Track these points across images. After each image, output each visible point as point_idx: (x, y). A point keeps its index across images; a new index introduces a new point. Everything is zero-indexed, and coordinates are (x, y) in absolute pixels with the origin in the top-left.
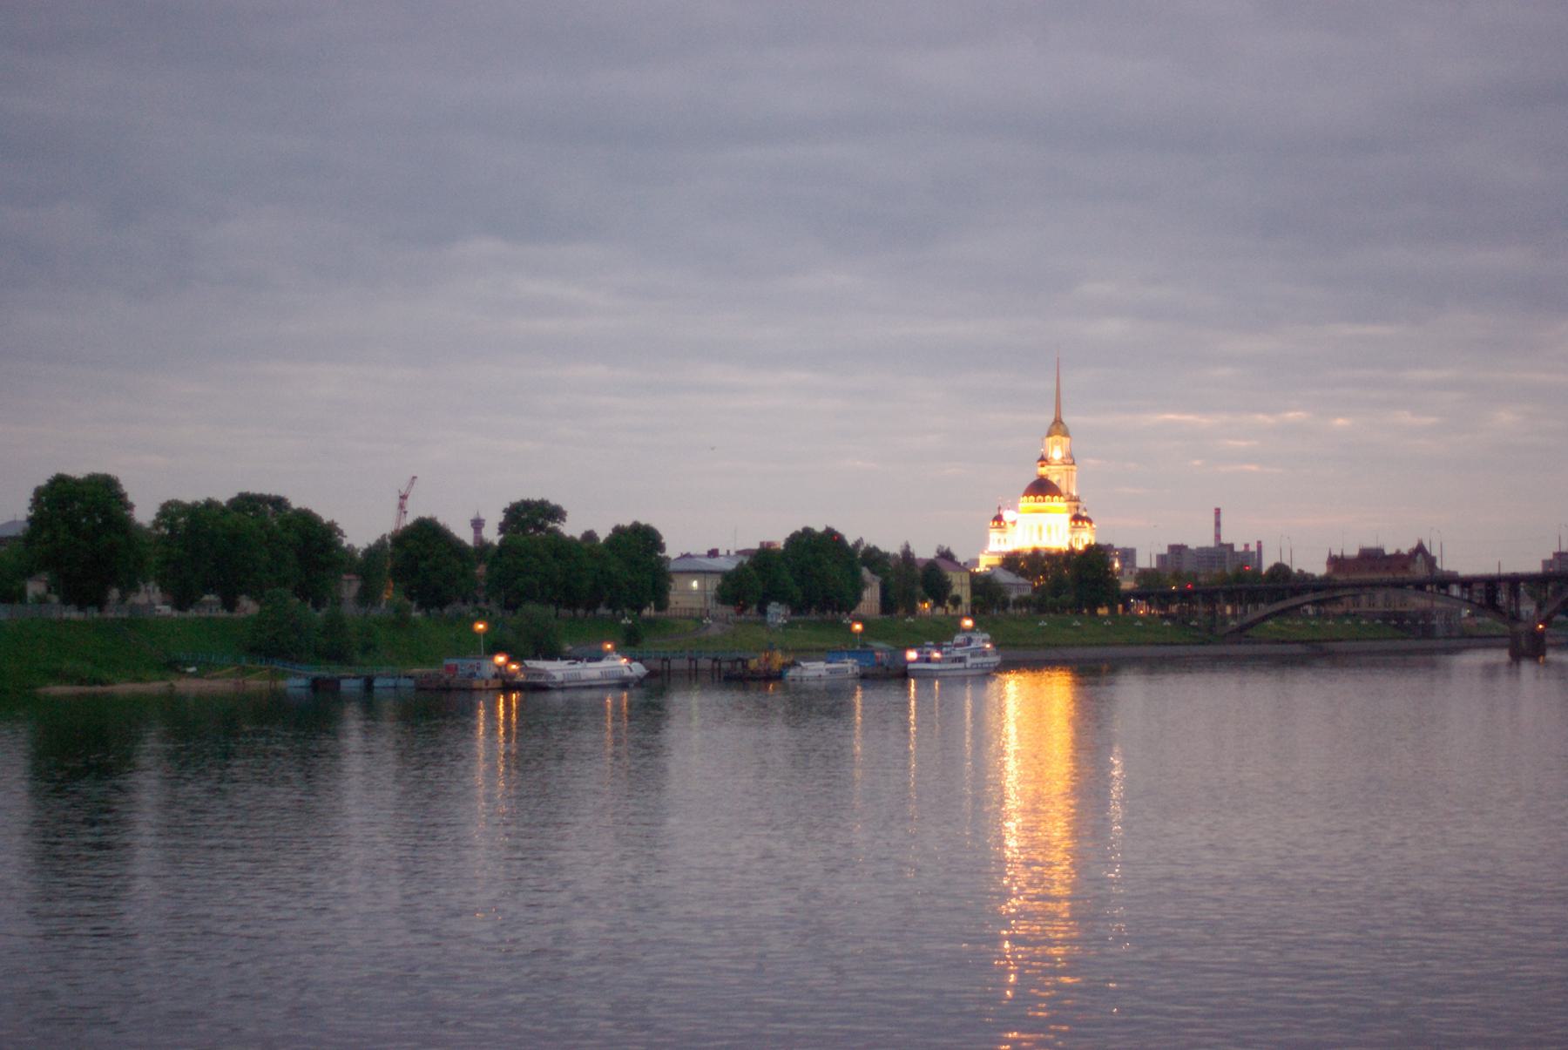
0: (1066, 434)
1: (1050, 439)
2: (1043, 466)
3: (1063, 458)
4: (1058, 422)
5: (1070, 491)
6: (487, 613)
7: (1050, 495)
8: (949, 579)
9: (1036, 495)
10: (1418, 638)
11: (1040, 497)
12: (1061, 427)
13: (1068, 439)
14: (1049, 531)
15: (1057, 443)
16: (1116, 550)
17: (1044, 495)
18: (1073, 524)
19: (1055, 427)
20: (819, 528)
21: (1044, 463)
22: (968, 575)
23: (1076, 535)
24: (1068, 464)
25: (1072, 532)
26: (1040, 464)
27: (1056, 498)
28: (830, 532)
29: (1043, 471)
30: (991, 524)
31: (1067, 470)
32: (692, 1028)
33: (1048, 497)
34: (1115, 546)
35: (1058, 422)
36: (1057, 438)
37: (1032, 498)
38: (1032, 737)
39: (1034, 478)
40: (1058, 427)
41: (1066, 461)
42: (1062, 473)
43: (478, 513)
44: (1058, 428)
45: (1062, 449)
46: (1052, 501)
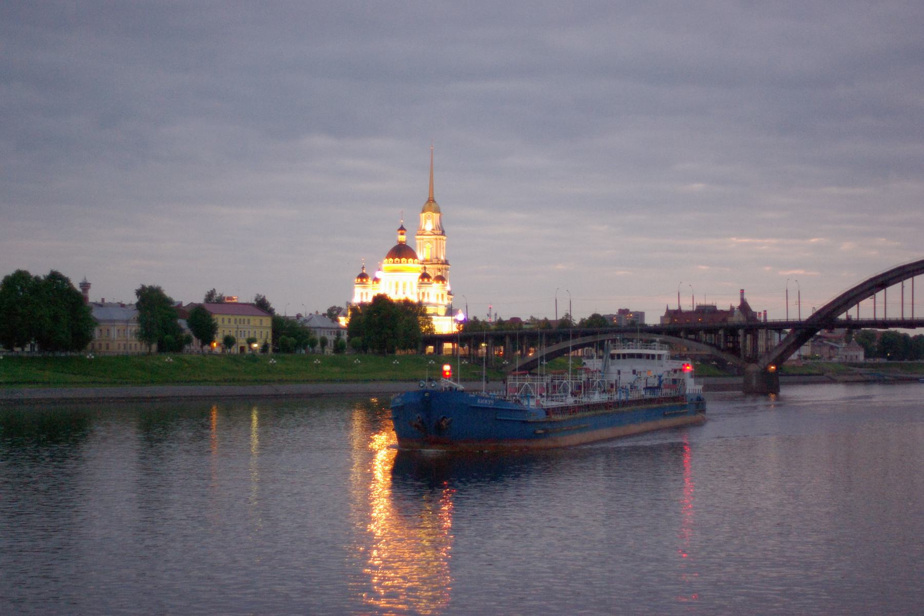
0: (437, 211)
1: (424, 214)
2: (402, 234)
3: (433, 230)
4: (431, 200)
5: (439, 257)
6: (412, 340)
7: (406, 258)
8: (215, 321)
9: (393, 258)
10: (733, 376)
11: (397, 259)
12: (433, 205)
13: (439, 215)
14: (404, 286)
15: (428, 218)
16: (631, 313)
17: (400, 257)
18: (421, 280)
19: (428, 204)
20: (376, 295)
21: (403, 231)
22: (267, 322)
23: (423, 290)
24: (437, 235)
25: (420, 287)
26: (400, 232)
27: (411, 260)
28: (55, 277)
29: (402, 238)
30: (356, 280)
31: (436, 239)
32: (682, 411)
33: (403, 259)
34: (631, 311)
35: (431, 200)
36: (429, 213)
37: (391, 260)
38: (363, 456)
39: (394, 244)
40: (431, 204)
41: (436, 232)
42: (432, 242)
43: (85, 279)
44: (430, 205)
45: (433, 224)
46: (407, 262)
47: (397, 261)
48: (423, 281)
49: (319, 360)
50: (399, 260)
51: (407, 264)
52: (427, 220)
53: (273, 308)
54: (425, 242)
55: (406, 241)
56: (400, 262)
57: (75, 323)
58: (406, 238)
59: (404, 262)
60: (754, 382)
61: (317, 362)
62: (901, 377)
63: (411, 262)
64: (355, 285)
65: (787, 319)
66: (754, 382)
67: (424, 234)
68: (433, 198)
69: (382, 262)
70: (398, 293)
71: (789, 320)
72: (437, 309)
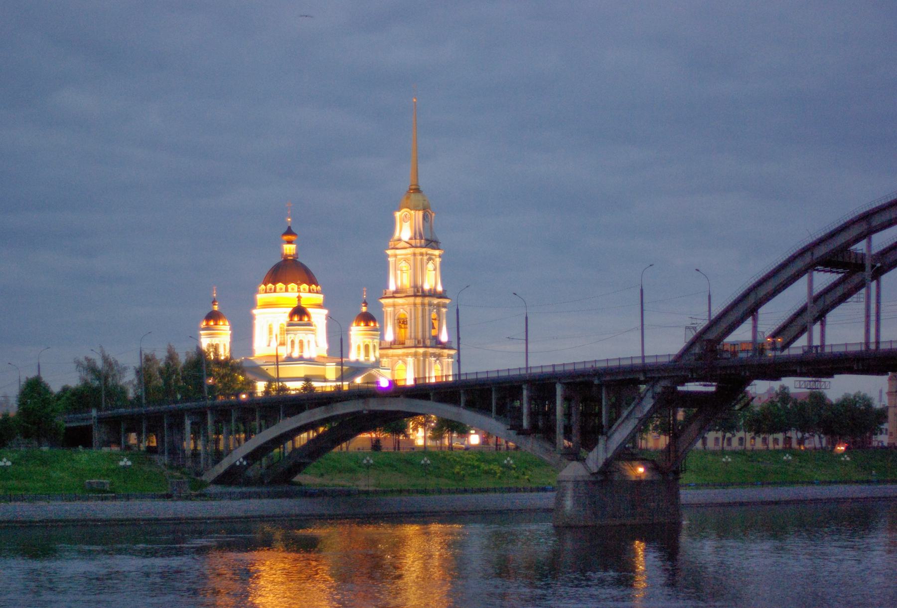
15: (404, 219)
26: (286, 238)
33: (280, 285)
46: (287, 290)
47: (281, 289)
48: (301, 320)
49: (789, 455)
50: (273, 287)
51: (287, 294)
52: (403, 223)
53: (843, 394)
54: (400, 260)
55: (297, 254)
56: (287, 290)
57: (118, 403)
58: (297, 249)
59: (293, 289)
60: (569, 503)
61: (788, 457)
62: (92, 501)
63: (304, 289)
64: (202, 332)
65: (643, 357)
66: (569, 503)
67: (397, 246)
68: (417, 185)
69: (256, 291)
70: (318, 345)
71: (647, 361)
72: (325, 369)
